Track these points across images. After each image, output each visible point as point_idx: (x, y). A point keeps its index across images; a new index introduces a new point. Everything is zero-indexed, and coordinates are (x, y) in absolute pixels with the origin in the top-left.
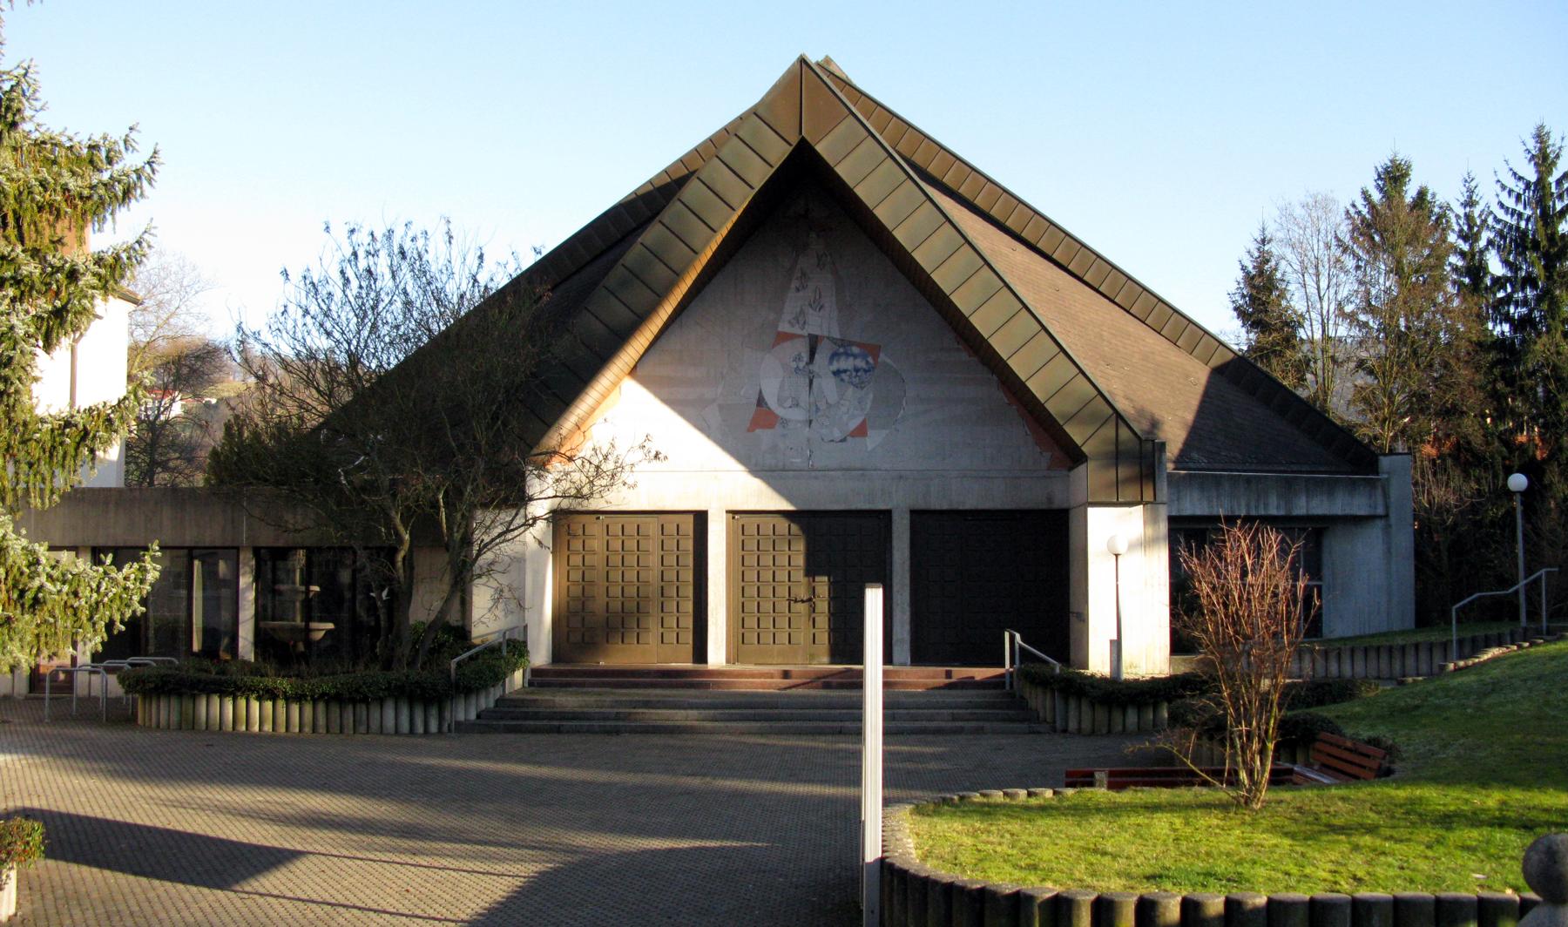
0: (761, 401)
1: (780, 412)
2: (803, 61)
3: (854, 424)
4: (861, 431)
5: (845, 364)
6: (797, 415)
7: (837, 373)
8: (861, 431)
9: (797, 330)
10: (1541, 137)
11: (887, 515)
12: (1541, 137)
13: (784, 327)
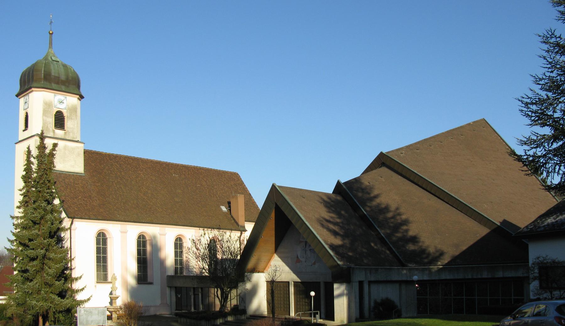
1: (301, 259)
3: (313, 261)
6: (303, 260)
8: (314, 264)
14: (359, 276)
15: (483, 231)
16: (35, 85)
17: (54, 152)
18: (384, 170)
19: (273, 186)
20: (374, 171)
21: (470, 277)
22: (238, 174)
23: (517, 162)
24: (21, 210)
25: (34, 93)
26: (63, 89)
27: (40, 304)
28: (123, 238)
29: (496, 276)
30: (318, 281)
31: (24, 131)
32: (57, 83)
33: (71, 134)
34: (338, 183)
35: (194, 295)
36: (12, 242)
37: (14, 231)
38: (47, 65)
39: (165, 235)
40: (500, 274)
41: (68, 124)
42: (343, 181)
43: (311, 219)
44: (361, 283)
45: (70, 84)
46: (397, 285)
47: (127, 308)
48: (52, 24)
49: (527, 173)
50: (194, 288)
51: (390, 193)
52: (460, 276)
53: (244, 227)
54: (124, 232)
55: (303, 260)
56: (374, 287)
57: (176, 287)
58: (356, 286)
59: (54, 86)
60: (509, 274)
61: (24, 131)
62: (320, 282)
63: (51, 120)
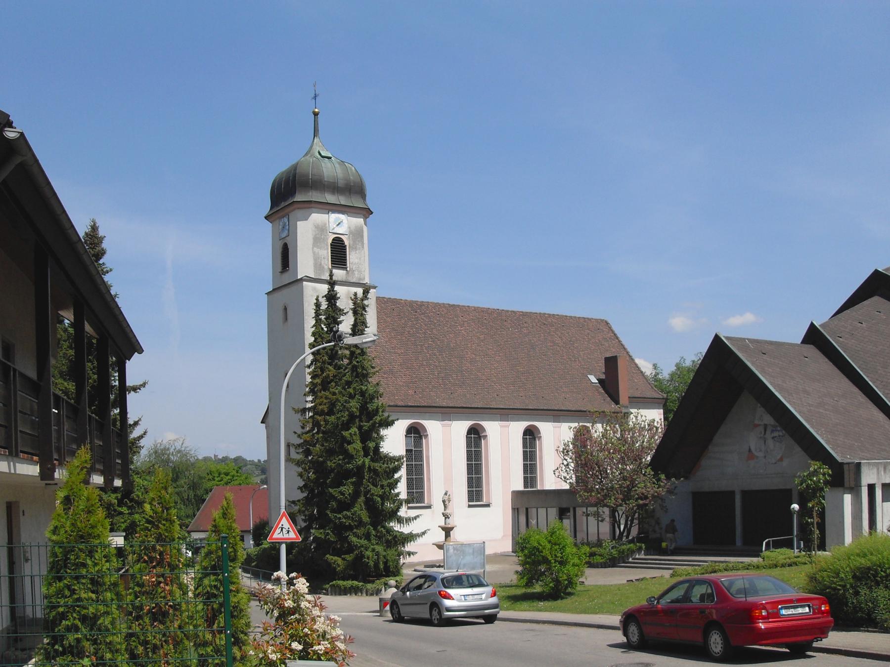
0: (750, 450)
1: (756, 454)
2: (717, 339)
3: (779, 457)
4: (781, 459)
5: (776, 434)
6: (761, 454)
7: (773, 438)
8: (781, 459)
9: (760, 423)
10: (140, 420)
11: (732, 493)
12: (140, 420)
13: (757, 422)
17: (366, 302)
19: (717, 339)
30: (788, 487)
33: (356, 273)
41: (352, 258)
44: (871, 488)
45: (351, 194)
47: (156, 452)
48: (313, 95)
55: (761, 454)
63: (326, 254)
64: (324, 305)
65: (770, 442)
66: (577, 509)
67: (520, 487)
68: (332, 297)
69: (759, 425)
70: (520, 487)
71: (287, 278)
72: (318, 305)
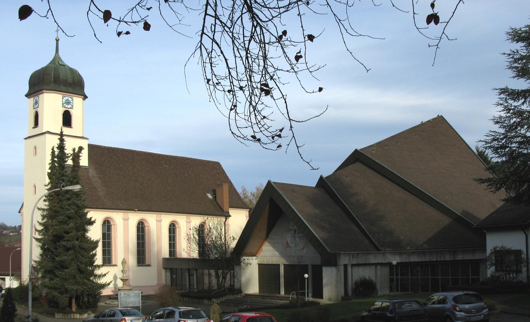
0: (287, 243)
3: (302, 247)
5: (300, 235)
6: (293, 245)
7: (299, 237)
8: (303, 249)
13: (290, 228)
14: (344, 260)
15: (446, 221)
16: (46, 87)
18: (358, 165)
19: (269, 183)
20: (351, 166)
21: (435, 260)
22: (219, 163)
23: (482, 184)
24: (47, 203)
25: (45, 94)
26: (71, 91)
27: (75, 287)
28: (125, 224)
29: (457, 259)
31: (34, 128)
32: (65, 85)
34: (321, 177)
35: (189, 276)
36: (39, 231)
37: (40, 221)
38: (56, 70)
39: (161, 221)
40: (460, 257)
41: (75, 121)
42: (325, 176)
43: (301, 210)
44: (345, 266)
46: (373, 267)
49: (491, 190)
50: (189, 270)
51: (367, 188)
52: (427, 259)
53: (228, 212)
54: (126, 220)
56: (355, 269)
57: (171, 269)
58: (342, 268)
59: (63, 88)
60: (468, 257)
61: (34, 128)
62: (307, 265)
64: (57, 151)
65: (297, 239)
66: (198, 271)
67: (167, 256)
68: (61, 147)
69: (292, 230)
70: (167, 256)
71: (37, 131)
72: (53, 152)
